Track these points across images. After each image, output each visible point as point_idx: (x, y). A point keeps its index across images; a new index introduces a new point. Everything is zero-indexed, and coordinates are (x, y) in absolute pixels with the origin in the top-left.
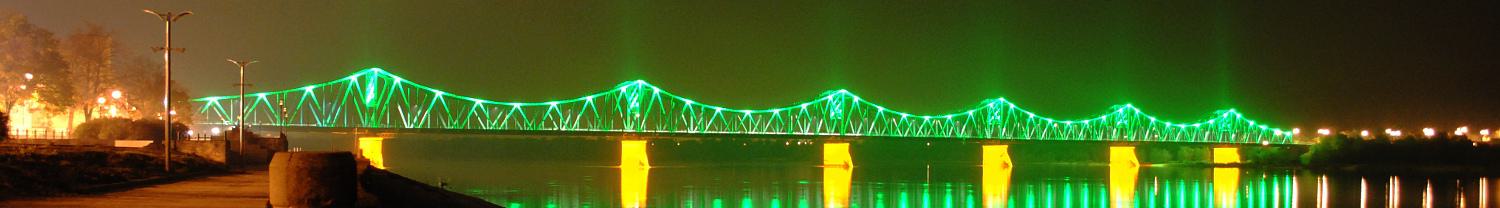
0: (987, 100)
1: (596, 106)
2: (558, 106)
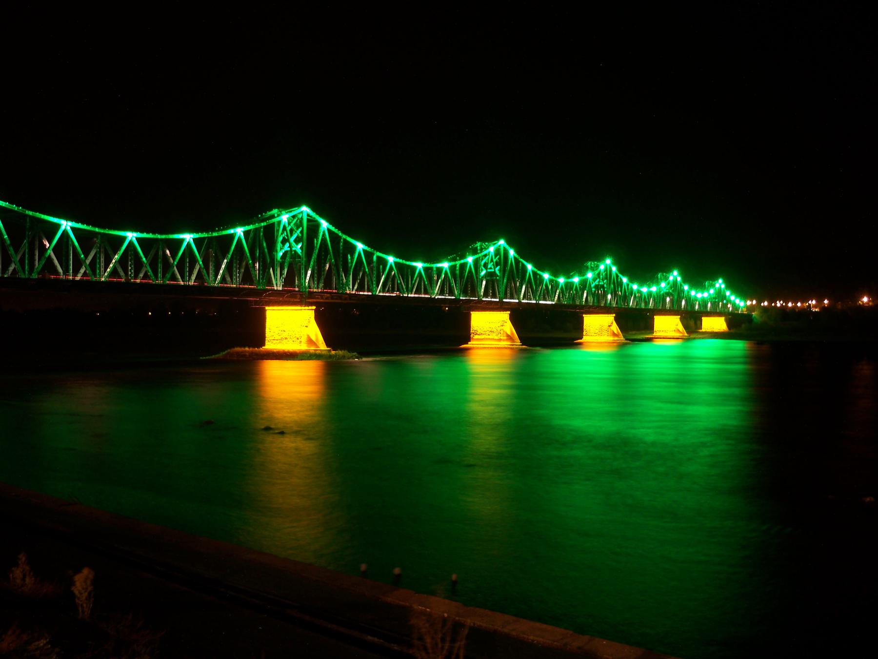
0: (275, 211)
1: (409, 266)
2: (138, 239)
